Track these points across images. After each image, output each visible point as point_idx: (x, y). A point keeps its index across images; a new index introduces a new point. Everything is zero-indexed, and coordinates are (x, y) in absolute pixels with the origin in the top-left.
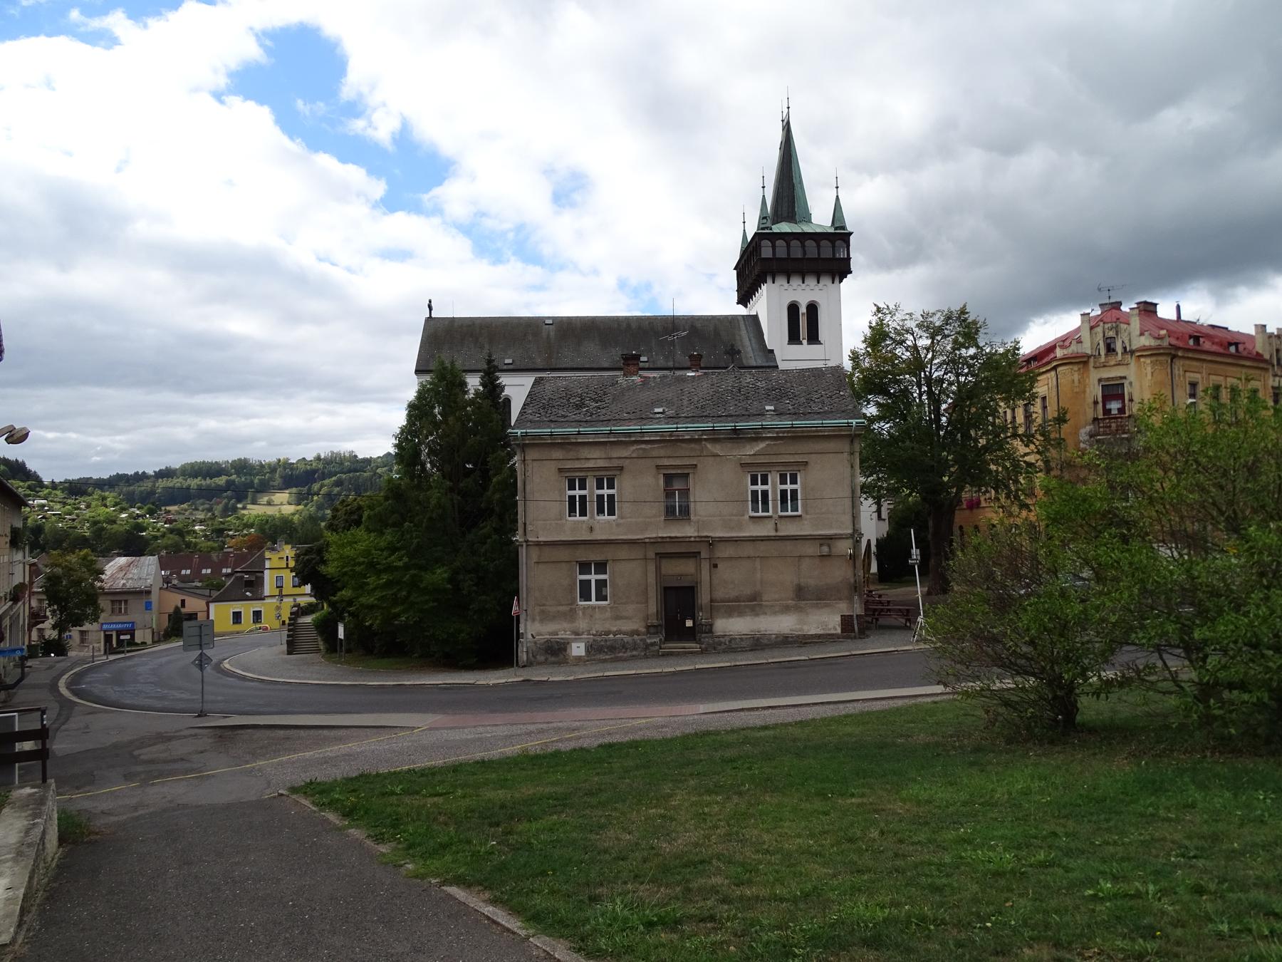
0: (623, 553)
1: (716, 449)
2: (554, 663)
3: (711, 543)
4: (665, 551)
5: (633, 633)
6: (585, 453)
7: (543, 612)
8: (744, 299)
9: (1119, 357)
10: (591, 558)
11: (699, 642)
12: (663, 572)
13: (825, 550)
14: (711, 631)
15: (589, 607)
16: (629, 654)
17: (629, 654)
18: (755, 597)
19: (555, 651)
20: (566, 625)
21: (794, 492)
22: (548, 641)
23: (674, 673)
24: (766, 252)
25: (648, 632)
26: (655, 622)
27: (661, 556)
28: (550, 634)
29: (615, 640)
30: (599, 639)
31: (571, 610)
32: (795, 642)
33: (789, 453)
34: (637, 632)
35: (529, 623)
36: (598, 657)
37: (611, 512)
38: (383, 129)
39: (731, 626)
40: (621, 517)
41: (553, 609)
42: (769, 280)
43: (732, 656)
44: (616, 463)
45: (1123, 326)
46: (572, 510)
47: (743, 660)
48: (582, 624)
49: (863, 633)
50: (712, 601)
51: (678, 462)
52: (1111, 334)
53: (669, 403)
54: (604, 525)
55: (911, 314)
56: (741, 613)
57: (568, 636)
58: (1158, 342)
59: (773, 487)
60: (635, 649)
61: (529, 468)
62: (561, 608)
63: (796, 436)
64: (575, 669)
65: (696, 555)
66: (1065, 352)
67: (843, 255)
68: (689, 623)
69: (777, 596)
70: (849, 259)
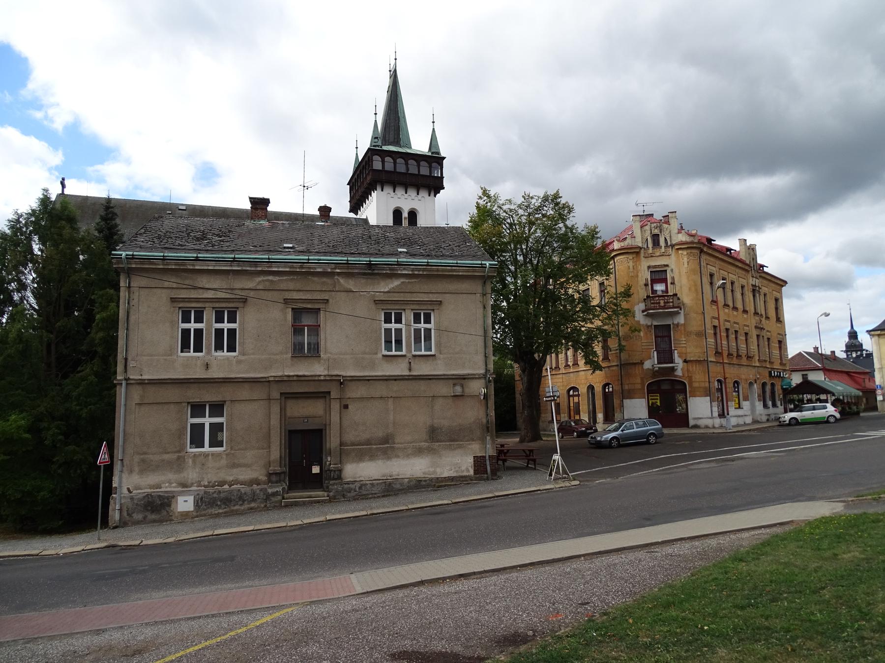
0: (244, 393)
1: (350, 284)
2: (154, 521)
3: (342, 382)
4: (292, 391)
5: (251, 482)
6: (203, 281)
7: (143, 461)
8: (356, 204)
9: (663, 250)
10: (205, 399)
11: (328, 490)
12: (289, 414)
13: (458, 389)
14: (340, 477)
15: (201, 454)
16: (246, 506)
17: (246, 506)
18: (387, 440)
19: (157, 507)
20: (171, 476)
21: (428, 331)
22: (148, 495)
23: (301, 527)
24: (377, 165)
25: (270, 481)
26: (278, 469)
28: (151, 487)
29: (231, 492)
30: (211, 490)
31: (179, 458)
33: (424, 292)
34: (257, 482)
35: (125, 476)
36: (210, 511)
37: (232, 348)
38: (60, 121)
39: (362, 471)
40: (243, 353)
41: (157, 458)
42: (379, 188)
43: (365, 503)
45: (665, 226)
46: (185, 347)
48: (191, 474)
49: (495, 475)
50: (341, 444)
51: (308, 296)
52: (656, 231)
53: (299, 242)
54: (221, 362)
55: (510, 201)
56: (372, 457)
57: (174, 488)
58: (691, 239)
59: (407, 326)
60: (254, 500)
61: (135, 296)
62: (166, 457)
63: (431, 275)
64: (179, 527)
65: (324, 395)
66: (622, 244)
67: (437, 174)
68: (316, 470)
69: (409, 438)
70: (442, 177)
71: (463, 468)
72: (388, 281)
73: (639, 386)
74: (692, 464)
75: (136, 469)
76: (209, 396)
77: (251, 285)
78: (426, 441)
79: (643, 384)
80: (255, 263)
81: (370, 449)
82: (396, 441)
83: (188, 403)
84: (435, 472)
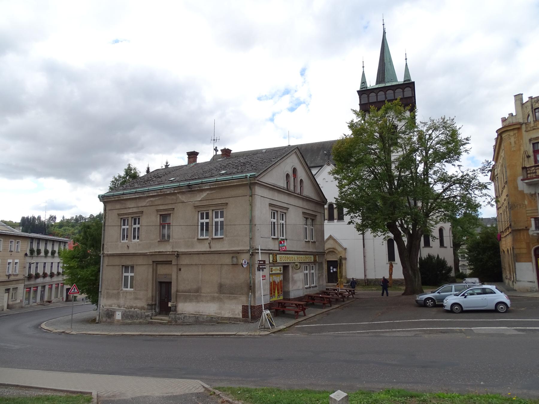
0: (140, 261)
1: (182, 198)
3: (178, 255)
4: (159, 261)
12: (158, 272)
14: (175, 310)
18: (198, 290)
20: (115, 301)
22: (108, 310)
27: (157, 263)
29: (134, 312)
32: (207, 322)
39: (186, 308)
44: (141, 209)
47: (195, 331)
48: (122, 302)
50: (177, 291)
60: (141, 318)
71: (236, 312)
72: (201, 193)
73: (524, 251)
74: (383, 332)
75: (105, 296)
76: (128, 262)
77: (144, 204)
78: (217, 293)
79: (529, 248)
80: (143, 192)
81: (190, 295)
82: (202, 292)
83: (123, 266)
84: (221, 313)
